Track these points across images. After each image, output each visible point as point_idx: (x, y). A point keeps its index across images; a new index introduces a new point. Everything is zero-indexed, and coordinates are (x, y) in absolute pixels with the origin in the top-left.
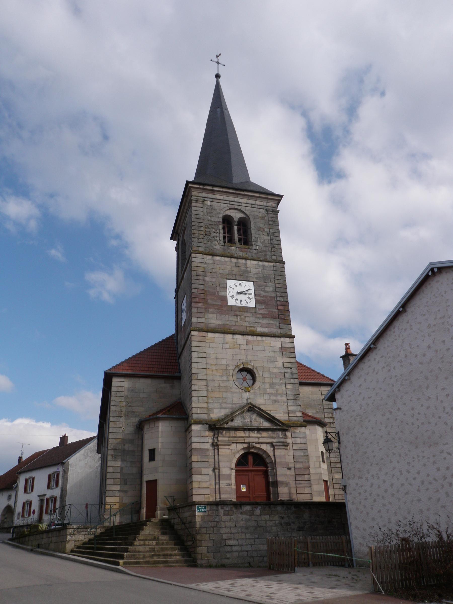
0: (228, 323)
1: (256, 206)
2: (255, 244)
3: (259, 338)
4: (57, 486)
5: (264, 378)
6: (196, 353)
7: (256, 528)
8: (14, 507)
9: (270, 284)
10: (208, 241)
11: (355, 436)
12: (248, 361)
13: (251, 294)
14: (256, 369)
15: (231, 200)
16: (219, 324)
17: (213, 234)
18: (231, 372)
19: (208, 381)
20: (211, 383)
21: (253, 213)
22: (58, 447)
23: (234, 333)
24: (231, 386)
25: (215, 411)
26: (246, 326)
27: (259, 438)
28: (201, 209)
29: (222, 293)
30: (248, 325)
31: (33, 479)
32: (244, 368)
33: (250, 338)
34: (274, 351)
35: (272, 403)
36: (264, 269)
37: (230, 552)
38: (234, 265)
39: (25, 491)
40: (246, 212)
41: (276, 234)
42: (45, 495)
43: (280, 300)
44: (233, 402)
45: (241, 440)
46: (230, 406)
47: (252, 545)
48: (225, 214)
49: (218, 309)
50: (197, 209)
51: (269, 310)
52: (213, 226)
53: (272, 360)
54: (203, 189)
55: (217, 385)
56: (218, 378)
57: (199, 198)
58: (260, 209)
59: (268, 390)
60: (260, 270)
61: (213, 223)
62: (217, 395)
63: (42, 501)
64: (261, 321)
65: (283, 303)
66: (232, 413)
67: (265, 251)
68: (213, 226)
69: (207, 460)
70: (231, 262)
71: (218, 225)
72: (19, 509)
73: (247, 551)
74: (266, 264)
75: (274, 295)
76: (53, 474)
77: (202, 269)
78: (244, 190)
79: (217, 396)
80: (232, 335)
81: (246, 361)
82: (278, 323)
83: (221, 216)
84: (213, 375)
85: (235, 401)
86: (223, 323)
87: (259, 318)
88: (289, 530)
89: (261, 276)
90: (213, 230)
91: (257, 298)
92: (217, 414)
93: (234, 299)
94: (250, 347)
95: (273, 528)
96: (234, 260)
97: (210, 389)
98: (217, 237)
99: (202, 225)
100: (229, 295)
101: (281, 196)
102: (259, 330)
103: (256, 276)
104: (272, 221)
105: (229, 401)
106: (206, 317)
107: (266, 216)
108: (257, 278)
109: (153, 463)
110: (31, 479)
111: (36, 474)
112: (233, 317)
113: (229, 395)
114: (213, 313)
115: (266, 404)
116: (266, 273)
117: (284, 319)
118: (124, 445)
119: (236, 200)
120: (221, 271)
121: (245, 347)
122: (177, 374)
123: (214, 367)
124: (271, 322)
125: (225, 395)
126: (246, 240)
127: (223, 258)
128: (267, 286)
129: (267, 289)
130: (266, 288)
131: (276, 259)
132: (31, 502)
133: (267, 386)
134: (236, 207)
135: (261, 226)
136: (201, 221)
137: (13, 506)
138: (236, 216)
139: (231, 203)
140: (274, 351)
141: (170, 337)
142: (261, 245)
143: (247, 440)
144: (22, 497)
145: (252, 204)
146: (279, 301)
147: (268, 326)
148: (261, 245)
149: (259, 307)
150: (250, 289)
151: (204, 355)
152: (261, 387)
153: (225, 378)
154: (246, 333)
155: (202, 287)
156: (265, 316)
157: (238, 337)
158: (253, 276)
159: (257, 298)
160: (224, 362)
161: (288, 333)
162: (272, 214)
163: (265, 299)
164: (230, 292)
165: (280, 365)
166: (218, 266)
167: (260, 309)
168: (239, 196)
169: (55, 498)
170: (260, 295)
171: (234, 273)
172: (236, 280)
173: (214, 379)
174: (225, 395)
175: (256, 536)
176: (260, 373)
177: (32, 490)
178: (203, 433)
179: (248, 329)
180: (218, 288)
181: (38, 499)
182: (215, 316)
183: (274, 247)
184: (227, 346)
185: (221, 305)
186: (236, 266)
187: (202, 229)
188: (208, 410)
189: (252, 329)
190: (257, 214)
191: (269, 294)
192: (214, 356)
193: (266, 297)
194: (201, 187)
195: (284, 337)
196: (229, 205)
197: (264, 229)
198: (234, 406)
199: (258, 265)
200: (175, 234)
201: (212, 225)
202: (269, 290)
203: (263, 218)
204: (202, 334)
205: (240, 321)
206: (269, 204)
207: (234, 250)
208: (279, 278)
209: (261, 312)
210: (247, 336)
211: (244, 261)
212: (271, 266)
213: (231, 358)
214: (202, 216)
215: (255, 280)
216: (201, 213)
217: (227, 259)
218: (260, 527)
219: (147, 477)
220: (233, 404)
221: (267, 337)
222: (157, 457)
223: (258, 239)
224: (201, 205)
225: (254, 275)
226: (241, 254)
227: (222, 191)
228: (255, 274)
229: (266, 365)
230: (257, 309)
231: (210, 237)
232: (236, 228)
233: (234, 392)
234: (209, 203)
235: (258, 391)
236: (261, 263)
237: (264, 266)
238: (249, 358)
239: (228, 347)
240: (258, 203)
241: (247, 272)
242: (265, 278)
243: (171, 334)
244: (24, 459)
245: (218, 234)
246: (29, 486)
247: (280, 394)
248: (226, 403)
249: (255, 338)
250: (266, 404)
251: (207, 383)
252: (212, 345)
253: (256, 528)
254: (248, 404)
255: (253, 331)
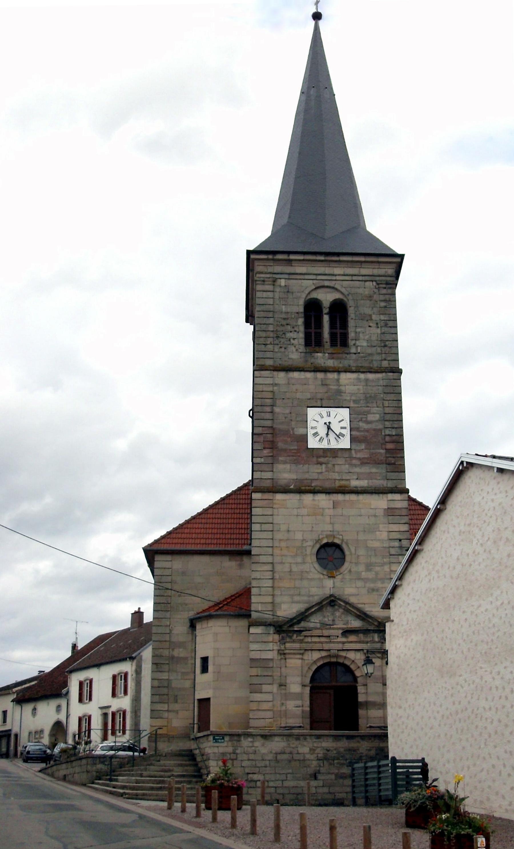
0: (307, 476)
1: (360, 278)
2: (354, 345)
3: (353, 497)
4: (126, 693)
5: (358, 556)
6: (258, 525)
7: (290, 761)
8: (67, 723)
9: (375, 410)
10: (281, 347)
11: (400, 657)
12: (335, 533)
13: (345, 428)
14: (347, 544)
15: (318, 272)
16: (293, 479)
17: (289, 335)
18: (309, 550)
19: (275, 565)
20: (278, 568)
21: (353, 291)
22: (128, 629)
23: (314, 492)
24: (308, 570)
25: (284, 606)
26: (335, 480)
27: (343, 643)
28: (270, 295)
29: (300, 431)
30: (338, 478)
31: (91, 681)
32: (327, 543)
33: (340, 497)
34: (375, 516)
35: (368, 592)
36: (367, 385)
37: (254, 787)
38: (320, 383)
39: (81, 700)
40: (343, 290)
41: (391, 324)
42: (109, 707)
43: (390, 433)
44: (311, 594)
45: (318, 646)
46: (305, 598)
47: (283, 781)
48: (309, 297)
49: (293, 456)
50: (265, 295)
51: (372, 451)
52: (288, 321)
53: (371, 530)
54: (273, 260)
55: (287, 569)
56: (290, 560)
57: (268, 276)
58: (365, 281)
59: (363, 573)
60: (361, 387)
61: (289, 316)
62: (285, 584)
63: (105, 715)
64: (357, 470)
65: (394, 438)
66: (307, 610)
67: (371, 355)
68: (288, 321)
69: (270, 674)
70: (316, 378)
71: (297, 319)
72: (73, 727)
73: (276, 787)
74: (371, 376)
75: (380, 426)
76: (119, 674)
77: (270, 395)
78: (338, 254)
79: (287, 585)
80: (311, 495)
81: (331, 533)
82: (384, 471)
83: (302, 302)
84: (282, 556)
85: (314, 590)
86: (300, 477)
87: (355, 466)
88: (336, 765)
89: (362, 397)
90: (289, 328)
91: (353, 433)
92: (287, 610)
93: (318, 438)
94: (339, 511)
95: (314, 762)
96: (320, 375)
97: (277, 576)
98: (294, 339)
99: (271, 321)
100: (310, 432)
101: (402, 256)
102: (355, 483)
103: (353, 398)
104: (385, 301)
105: (303, 592)
106: (274, 470)
107: (375, 293)
108: (355, 401)
109: (205, 675)
110: (88, 682)
111: (92, 674)
112: (316, 466)
113: (305, 583)
114: (285, 463)
115: (358, 595)
116: (370, 392)
117: (394, 464)
118: (173, 650)
119: (328, 271)
120: (299, 395)
121: (331, 512)
122: (246, 547)
123: (283, 544)
124: (374, 470)
125: (298, 583)
126: (341, 340)
127: (302, 373)
128: (369, 413)
129: (370, 417)
130: (369, 415)
131: (387, 366)
132: (90, 717)
133: (361, 568)
134: (327, 283)
135: (368, 311)
136: (271, 315)
137: (64, 721)
138: (326, 298)
139: (319, 277)
140: (375, 516)
141: (245, 485)
142: (365, 344)
143: (326, 646)
144: (77, 710)
145: (352, 275)
146: (389, 435)
147: (370, 476)
148: (365, 344)
149: (357, 448)
150: (343, 420)
151: (269, 527)
152: (352, 570)
153: (299, 559)
154: (334, 491)
155: (268, 423)
156: (363, 462)
157: (321, 497)
158: (348, 398)
159: (353, 433)
160: (299, 536)
161: (399, 486)
162: (385, 288)
163: (366, 434)
164: (312, 428)
165: (384, 535)
166: (294, 388)
167: (356, 451)
168: (332, 264)
169: (124, 712)
170: (358, 429)
171: (319, 396)
172: (322, 407)
173: (284, 561)
174: (298, 583)
175: (290, 771)
176: (353, 550)
177: (90, 699)
178: (265, 638)
179: (338, 484)
180: (293, 423)
181: (100, 712)
182: (288, 466)
183: (385, 346)
184: (305, 511)
185: (297, 450)
186: (322, 385)
187: (271, 328)
188: (273, 606)
189: (343, 483)
190: (361, 291)
191: (373, 426)
192: (283, 528)
193: (367, 431)
194: (270, 257)
195: (392, 493)
196: (315, 282)
197: (370, 316)
198: (311, 599)
199: (358, 379)
200: (250, 318)
201: (287, 319)
202: (374, 419)
203: (370, 298)
204: (267, 496)
205: (326, 471)
206: (382, 272)
207: (321, 358)
208: (392, 397)
209: (359, 455)
210: (335, 495)
211: (335, 375)
212: (378, 379)
213: (310, 529)
214: (271, 307)
215: (352, 405)
216: (271, 301)
217: (309, 375)
218: (296, 760)
219: (200, 695)
220: (309, 596)
221: (365, 495)
222: (210, 668)
223: (361, 335)
224: (270, 288)
225: (351, 396)
226: (330, 363)
227: (303, 260)
228: (352, 394)
229: (362, 537)
230: (353, 452)
231: (282, 340)
232: (326, 318)
233: (312, 579)
234: (283, 282)
235: (347, 577)
236: (362, 376)
237: (367, 380)
238: (337, 527)
239: (306, 514)
240: (364, 271)
241: (339, 392)
242: (369, 398)
243: (246, 481)
244: (80, 646)
245: (296, 333)
246: (86, 693)
247: (380, 579)
248: (299, 595)
249: (348, 497)
250: (358, 595)
251: (273, 567)
252: (282, 511)
253: (290, 761)
254: (331, 596)
255: (345, 487)
